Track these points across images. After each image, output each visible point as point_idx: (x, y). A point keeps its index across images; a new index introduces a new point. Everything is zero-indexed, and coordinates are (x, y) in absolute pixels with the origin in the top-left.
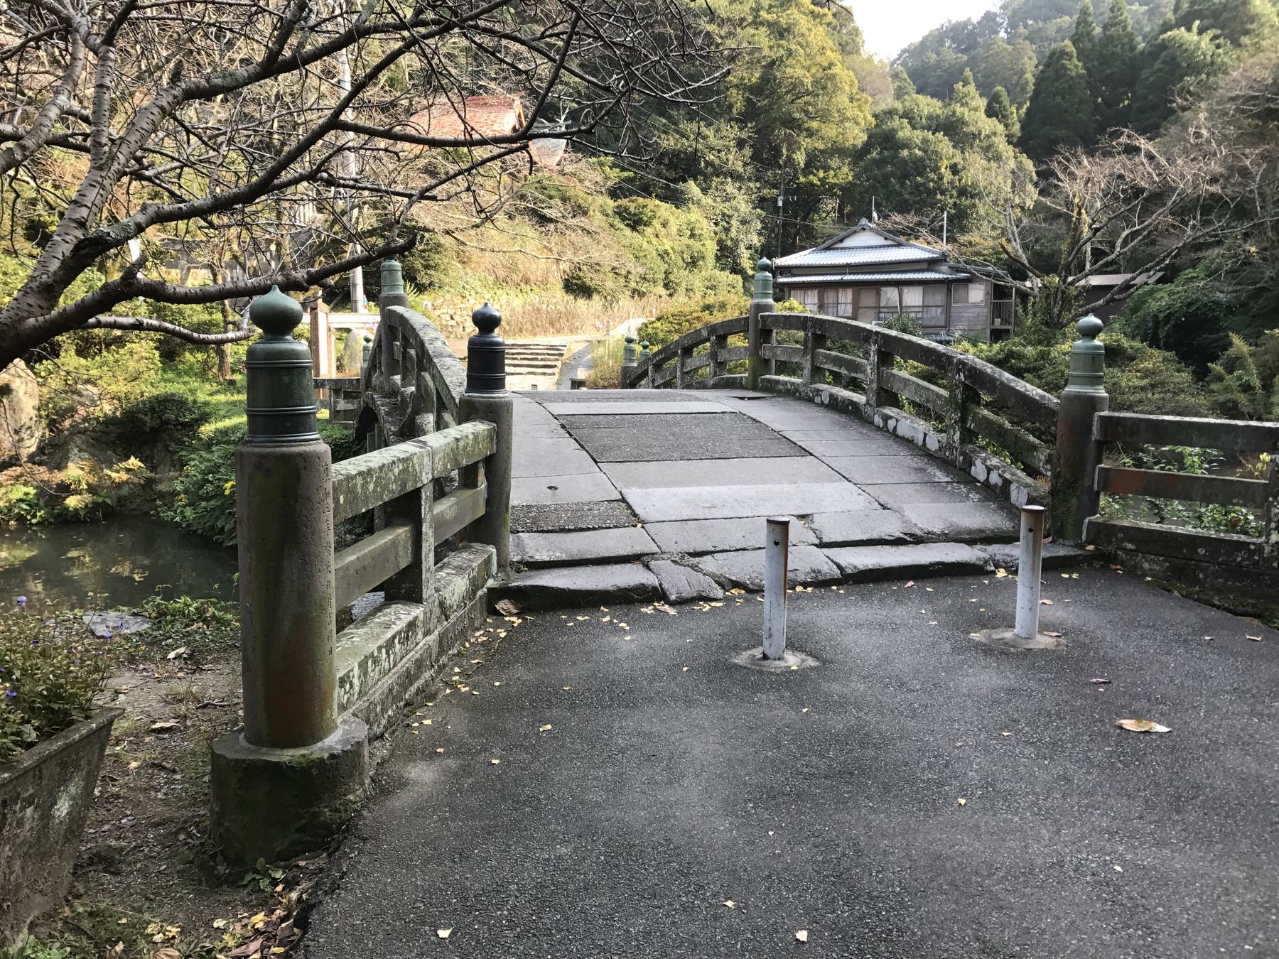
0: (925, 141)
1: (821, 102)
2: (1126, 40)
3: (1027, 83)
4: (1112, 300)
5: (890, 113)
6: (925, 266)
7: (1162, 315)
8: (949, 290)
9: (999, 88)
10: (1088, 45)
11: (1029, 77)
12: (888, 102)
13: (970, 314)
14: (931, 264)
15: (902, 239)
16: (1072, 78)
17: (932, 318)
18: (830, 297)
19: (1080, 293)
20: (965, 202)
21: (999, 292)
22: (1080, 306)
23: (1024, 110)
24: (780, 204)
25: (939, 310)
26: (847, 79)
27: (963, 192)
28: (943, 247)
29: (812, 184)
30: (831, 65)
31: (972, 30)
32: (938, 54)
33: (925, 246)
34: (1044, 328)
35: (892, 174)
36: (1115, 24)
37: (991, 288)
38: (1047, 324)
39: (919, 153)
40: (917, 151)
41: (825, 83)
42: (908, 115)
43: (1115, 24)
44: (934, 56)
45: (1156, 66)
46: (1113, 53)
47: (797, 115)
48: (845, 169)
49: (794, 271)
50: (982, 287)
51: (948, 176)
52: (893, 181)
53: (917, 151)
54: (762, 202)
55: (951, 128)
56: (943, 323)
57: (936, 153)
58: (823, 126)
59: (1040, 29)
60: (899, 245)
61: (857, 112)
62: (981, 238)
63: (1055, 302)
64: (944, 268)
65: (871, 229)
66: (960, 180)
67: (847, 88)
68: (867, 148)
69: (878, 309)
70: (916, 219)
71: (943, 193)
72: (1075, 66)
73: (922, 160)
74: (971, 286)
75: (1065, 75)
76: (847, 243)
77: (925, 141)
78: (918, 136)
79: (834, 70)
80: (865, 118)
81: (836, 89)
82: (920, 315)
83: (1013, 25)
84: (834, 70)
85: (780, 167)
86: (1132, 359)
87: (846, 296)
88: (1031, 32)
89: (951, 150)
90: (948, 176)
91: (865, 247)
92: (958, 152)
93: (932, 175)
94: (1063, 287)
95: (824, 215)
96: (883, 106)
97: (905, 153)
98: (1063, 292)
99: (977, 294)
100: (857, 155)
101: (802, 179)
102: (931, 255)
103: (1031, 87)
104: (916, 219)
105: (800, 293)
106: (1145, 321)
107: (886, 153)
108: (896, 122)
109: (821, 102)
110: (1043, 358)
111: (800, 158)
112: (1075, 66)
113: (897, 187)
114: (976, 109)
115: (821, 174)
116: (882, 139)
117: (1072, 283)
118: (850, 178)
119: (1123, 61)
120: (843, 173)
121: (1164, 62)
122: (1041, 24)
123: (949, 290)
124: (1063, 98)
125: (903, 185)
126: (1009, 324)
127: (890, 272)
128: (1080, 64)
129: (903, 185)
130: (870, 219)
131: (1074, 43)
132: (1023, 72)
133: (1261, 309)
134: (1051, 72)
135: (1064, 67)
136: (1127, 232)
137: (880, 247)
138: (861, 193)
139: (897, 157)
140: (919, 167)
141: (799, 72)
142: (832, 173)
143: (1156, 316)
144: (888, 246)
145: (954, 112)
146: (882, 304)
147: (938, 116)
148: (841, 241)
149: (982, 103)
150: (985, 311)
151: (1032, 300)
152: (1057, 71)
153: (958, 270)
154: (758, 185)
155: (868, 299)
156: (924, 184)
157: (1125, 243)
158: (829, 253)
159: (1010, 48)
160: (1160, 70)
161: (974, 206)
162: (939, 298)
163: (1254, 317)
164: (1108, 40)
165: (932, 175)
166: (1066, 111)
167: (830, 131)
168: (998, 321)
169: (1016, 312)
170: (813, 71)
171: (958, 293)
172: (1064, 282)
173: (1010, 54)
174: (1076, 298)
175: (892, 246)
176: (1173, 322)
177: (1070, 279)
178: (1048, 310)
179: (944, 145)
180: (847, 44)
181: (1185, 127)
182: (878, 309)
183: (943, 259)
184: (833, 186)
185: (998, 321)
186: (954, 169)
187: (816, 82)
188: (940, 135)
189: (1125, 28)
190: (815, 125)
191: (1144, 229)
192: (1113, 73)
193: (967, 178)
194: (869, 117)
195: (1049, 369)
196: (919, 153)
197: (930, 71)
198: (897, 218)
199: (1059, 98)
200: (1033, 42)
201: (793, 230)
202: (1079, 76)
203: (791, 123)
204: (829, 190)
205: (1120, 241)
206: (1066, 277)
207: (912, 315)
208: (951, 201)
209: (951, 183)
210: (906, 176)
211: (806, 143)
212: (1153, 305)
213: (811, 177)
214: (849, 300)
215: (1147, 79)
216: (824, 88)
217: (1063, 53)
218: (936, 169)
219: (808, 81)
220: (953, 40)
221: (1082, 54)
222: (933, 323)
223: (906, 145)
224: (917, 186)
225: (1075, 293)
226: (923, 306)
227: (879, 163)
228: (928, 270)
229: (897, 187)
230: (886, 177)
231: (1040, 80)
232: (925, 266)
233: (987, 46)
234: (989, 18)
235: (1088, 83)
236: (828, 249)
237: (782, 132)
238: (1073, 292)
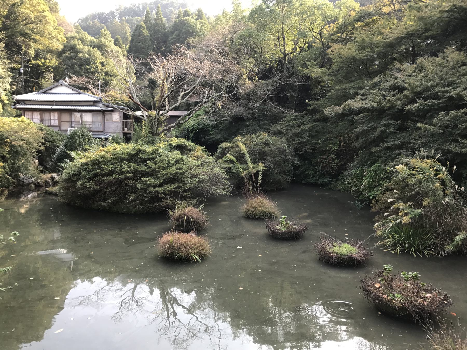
0: (89, 51)
1: (40, 27)
2: (162, 26)
3: (128, 37)
4: (179, 123)
5: (73, 38)
6: (92, 103)
7: (190, 129)
8: (104, 115)
9: (118, 36)
10: (150, 25)
11: (128, 34)
12: (74, 34)
13: (113, 126)
14: (95, 103)
15: (81, 91)
16: (145, 36)
17: (97, 127)
18: (46, 116)
19: (165, 120)
20: (108, 78)
21: (126, 117)
22: (165, 126)
23: (128, 46)
24: (22, 71)
25: (100, 124)
26: (52, 19)
27: (106, 74)
28: (99, 95)
29: (39, 65)
30: (43, 11)
31: (106, 16)
32: (93, 22)
33: (92, 95)
34: (151, 136)
35: (76, 64)
36: (159, 19)
37: (122, 115)
38: (152, 133)
39: (87, 56)
40: (86, 55)
41: (41, 19)
42: (81, 39)
43: (159, 19)
44: (91, 23)
45: (173, 37)
46: (158, 30)
47: (28, 31)
48: (54, 60)
49: (26, 102)
50: (118, 114)
51: (100, 67)
52: (73, 64)
53: (86, 55)
54: (12, 70)
55: (101, 47)
56: (102, 130)
57: (95, 56)
58: (41, 38)
59: (131, 20)
60: (79, 93)
61: (57, 34)
62: (116, 92)
63: (155, 123)
64: (101, 105)
65: (65, 85)
66: (105, 69)
67: (52, 22)
68: (63, 51)
69: (71, 122)
70: (86, 80)
71: (99, 73)
72: (146, 32)
73: (88, 59)
74: (113, 113)
75: (142, 35)
76: (53, 91)
77: (89, 51)
78: (86, 49)
79: (45, 14)
80: (61, 38)
81: (47, 23)
82: (91, 126)
83: (120, 17)
84: (45, 14)
85: (21, 55)
86: (190, 150)
87: (55, 116)
88: (127, 20)
89: (101, 57)
90: (100, 67)
91: (63, 93)
92: (104, 58)
93: (93, 66)
94: (158, 117)
95: (47, 80)
96: (69, 34)
97: (81, 55)
98: (158, 119)
99: (116, 117)
100: (60, 54)
101: (33, 62)
102: (96, 99)
103: (130, 38)
104: (86, 80)
105: (30, 113)
106: (184, 130)
107: (72, 54)
108: (76, 42)
109: (40, 27)
110: (156, 153)
111: (32, 52)
112: (146, 32)
113: (78, 69)
114: (110, 41)
115: (43, 61)
116: (70, 48)
117: (162, 115)
118: (57, 64)
119: (162, 33)
120: (53, 61)
121: (176, 35)
122: (131, 18)
123: (104, 115)
124: (142, 43)
125: (80, 68)
126: (131, 131)
127: (76, 106)
128: (147, 31)
129: (80, 68)
130: (65, 80)
131: (145, 23)
132: (126, 33)
133: (224, 127)
134: (137, 33)
135: (142, 31)
136: (183, 93)
137: (72, 94)
138: (62, 71)
139: (77, 56)
140: (87, 62)
141: (27, 11)
142: (48, 61)
143: (188, 129)
144: (74, 94)
145: (101, 41)
146: (73, 120)
147: (94, 42)
148: (51, 89)
149: (113, 41)
150: (120, 125)
151: (144, 122)
152: (139, 33)
153: (107, 106)
154: (9, 61)
155: (65, 117)
156: (90, 69)
157: (183, 98)
158: (45, 95)
159: (120, 24)
160: (174, 38)
161: (111, 80)
162: (99, 118)
163: (221, 130)
164: (156, 24)
165: (93, 66)
166: (143, 48)
167: (46, 41)
168: (126, 129)
169: (133, 125)
170: (35, 13)
171: (108, 116)
172: (158, 114)
173: (120, 26)
174: (163, 122)
175: (76, 94)
176: (194, 132)
177: (161, 112)
178: (152, 127)
179: (98, 54)
180: (53, 8)
181: (243, 33)
182: (71, 122)
183: (100, 101)
184: (48, 67)
185: (126, 129)
186: (103, 64)
187: (36, 17)
188: (96, 49)
189: (162, 21)
190: (37, 37)
191: (189, 92)
192: (158, 37)
193: (108, 68)
194: (64, 38)
195: (158, 159)
196: (87, 56)
197: (91, 26)
198: (75, 78)
199: (141, 43)
200: (128, 23)
201: (31, 85)
202: (147, 36)
203: (24, 34)
204: (47, 69)
205: (180, 97)
206: (159, 112)
207: (87, 126)
208: (102, 77)
209: (102, 69)
210: (82, 65)
211: (33, 45)
212: (187, 125)
213: (38, 61)
214: (56, 117)
215: (171, 40)
216: (41, 21)
217: (141, 26)
218: (95, 63)
219: (32, 16)
220: (99, 18)
221: (148, 28)
222: (97, 130)
223: (81, 52)
224: (87, 70)
225: (163, 120)
226: (92, 122)
227: (70, 58)
228: (93, 105)
229: (78, 69)
230: (73, 65)
231: (133, 36)
232: (92, 103)
233: (112, 22)
234: (112, 13)
235: (151, 39)
236: (44, 93)
237: (20, 39)
238: (162, 119)
